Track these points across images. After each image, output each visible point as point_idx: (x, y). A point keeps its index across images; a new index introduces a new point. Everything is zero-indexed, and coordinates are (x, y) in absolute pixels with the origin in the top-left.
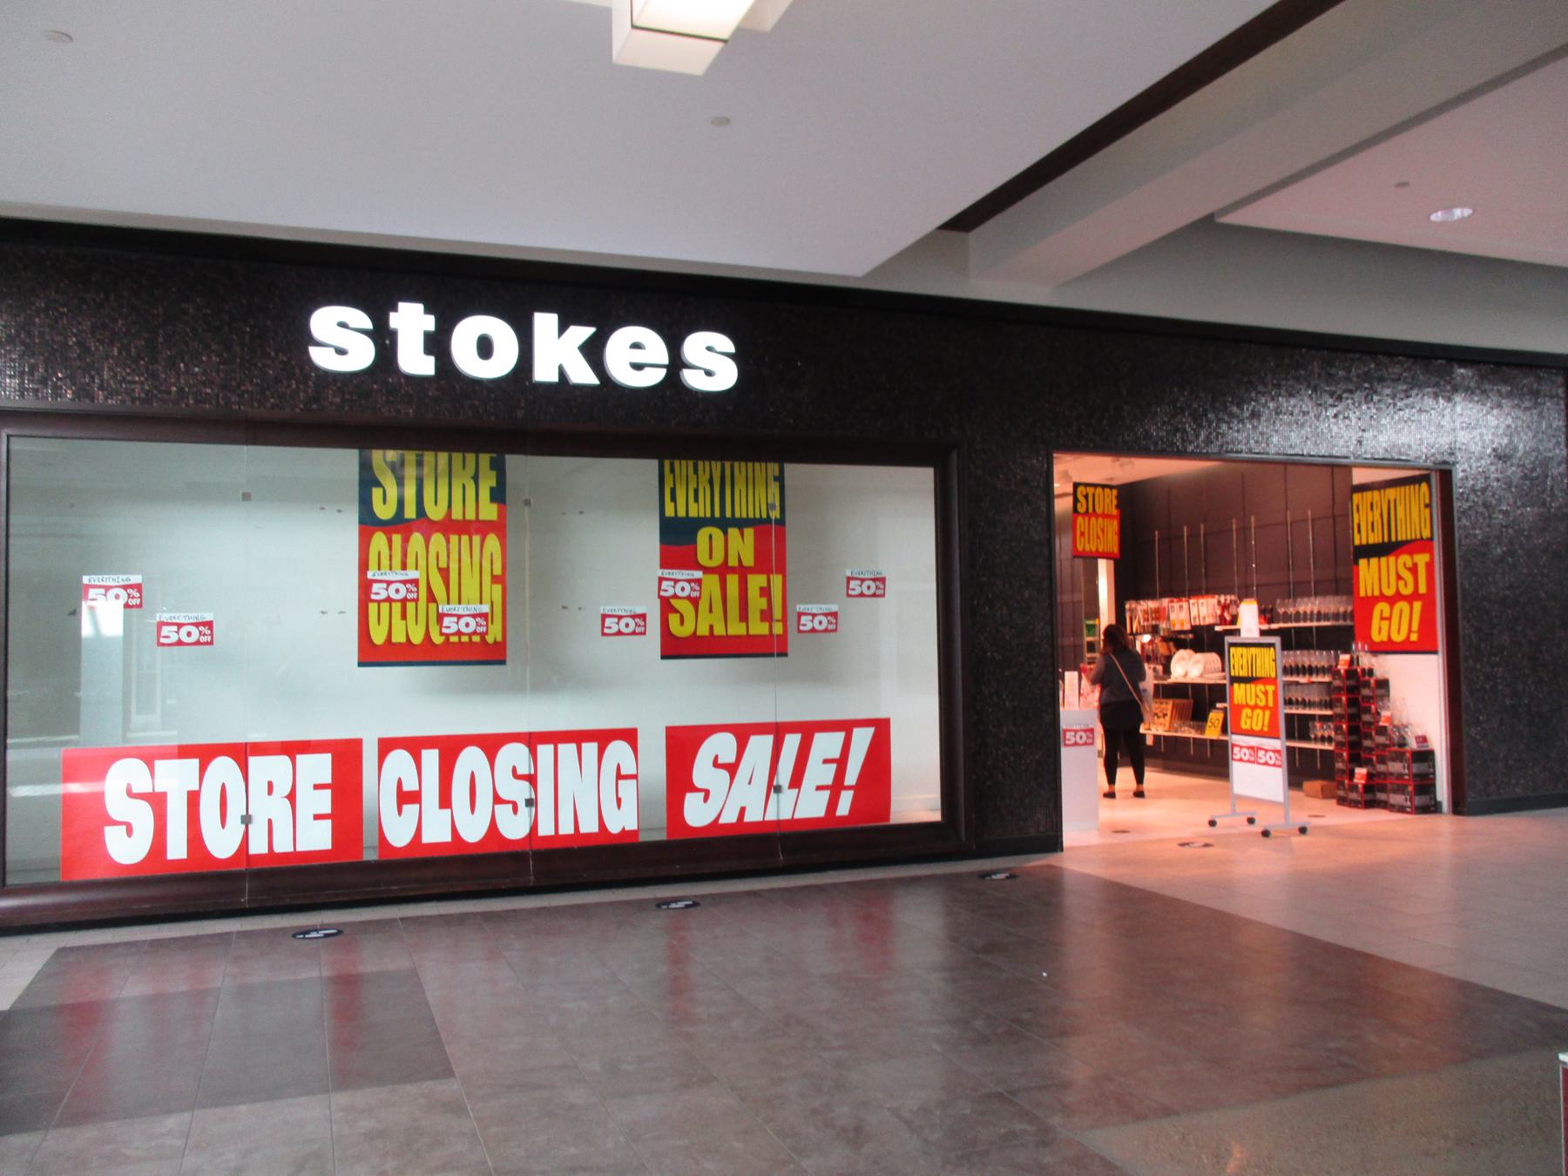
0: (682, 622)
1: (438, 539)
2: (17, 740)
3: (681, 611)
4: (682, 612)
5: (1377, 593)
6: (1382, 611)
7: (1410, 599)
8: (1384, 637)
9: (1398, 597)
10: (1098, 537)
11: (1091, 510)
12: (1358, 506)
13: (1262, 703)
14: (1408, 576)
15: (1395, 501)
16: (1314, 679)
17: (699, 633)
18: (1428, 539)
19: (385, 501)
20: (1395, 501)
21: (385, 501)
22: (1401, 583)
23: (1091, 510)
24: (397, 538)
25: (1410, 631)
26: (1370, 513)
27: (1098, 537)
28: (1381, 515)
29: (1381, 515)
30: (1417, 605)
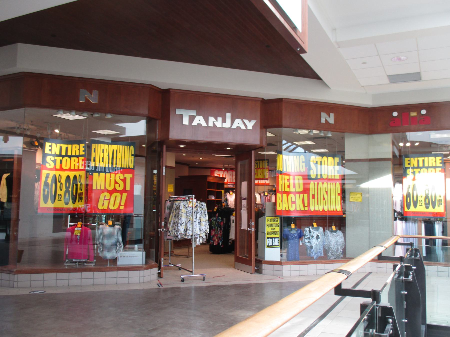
0: (119, 186)
1: (261, 170)
2: (417, 240)
3: (119, 183)
4: (119, 183)
5: (103, 188)
6: (105, 196)
7: (121, 192)
8: (105, 207)
9: (115, 190)
10: (261, 174)
11: (258, 167)
12: (95, 149)
13: (121, 188)
14: (122, 183)
15: (117, 150)
16: (246, 235)
17: (316, 210)
18: (132, 168)
19: (302, 159)
20: (117, 150)
21: (302, 159)
22: (117, 185)
23: (258, 167)
24: (257, 170)
25: (120, 205)
26: (102, 154)
27: (261, 174)
28: (109, 156)
29: (109, 156)
30: (125, 195)
